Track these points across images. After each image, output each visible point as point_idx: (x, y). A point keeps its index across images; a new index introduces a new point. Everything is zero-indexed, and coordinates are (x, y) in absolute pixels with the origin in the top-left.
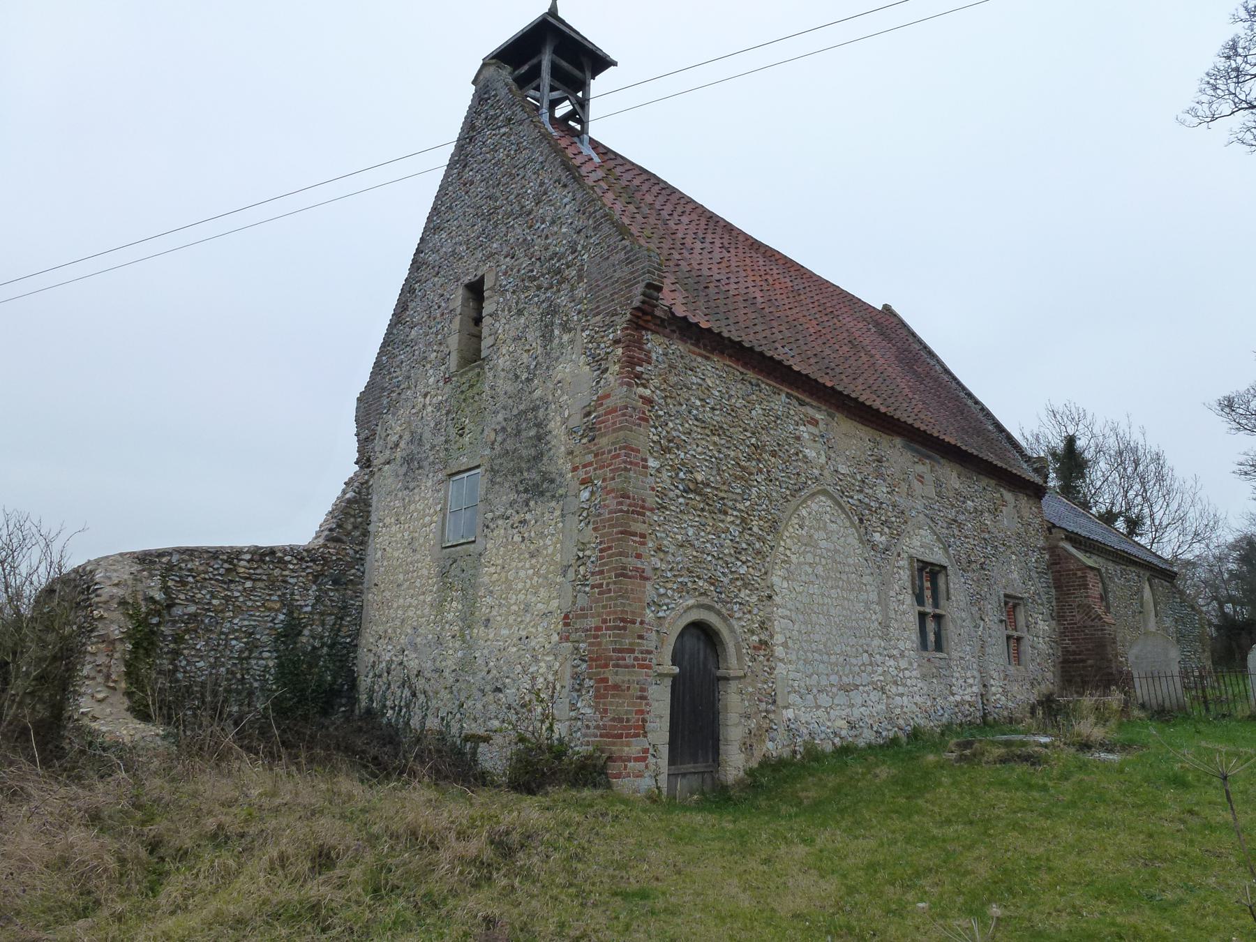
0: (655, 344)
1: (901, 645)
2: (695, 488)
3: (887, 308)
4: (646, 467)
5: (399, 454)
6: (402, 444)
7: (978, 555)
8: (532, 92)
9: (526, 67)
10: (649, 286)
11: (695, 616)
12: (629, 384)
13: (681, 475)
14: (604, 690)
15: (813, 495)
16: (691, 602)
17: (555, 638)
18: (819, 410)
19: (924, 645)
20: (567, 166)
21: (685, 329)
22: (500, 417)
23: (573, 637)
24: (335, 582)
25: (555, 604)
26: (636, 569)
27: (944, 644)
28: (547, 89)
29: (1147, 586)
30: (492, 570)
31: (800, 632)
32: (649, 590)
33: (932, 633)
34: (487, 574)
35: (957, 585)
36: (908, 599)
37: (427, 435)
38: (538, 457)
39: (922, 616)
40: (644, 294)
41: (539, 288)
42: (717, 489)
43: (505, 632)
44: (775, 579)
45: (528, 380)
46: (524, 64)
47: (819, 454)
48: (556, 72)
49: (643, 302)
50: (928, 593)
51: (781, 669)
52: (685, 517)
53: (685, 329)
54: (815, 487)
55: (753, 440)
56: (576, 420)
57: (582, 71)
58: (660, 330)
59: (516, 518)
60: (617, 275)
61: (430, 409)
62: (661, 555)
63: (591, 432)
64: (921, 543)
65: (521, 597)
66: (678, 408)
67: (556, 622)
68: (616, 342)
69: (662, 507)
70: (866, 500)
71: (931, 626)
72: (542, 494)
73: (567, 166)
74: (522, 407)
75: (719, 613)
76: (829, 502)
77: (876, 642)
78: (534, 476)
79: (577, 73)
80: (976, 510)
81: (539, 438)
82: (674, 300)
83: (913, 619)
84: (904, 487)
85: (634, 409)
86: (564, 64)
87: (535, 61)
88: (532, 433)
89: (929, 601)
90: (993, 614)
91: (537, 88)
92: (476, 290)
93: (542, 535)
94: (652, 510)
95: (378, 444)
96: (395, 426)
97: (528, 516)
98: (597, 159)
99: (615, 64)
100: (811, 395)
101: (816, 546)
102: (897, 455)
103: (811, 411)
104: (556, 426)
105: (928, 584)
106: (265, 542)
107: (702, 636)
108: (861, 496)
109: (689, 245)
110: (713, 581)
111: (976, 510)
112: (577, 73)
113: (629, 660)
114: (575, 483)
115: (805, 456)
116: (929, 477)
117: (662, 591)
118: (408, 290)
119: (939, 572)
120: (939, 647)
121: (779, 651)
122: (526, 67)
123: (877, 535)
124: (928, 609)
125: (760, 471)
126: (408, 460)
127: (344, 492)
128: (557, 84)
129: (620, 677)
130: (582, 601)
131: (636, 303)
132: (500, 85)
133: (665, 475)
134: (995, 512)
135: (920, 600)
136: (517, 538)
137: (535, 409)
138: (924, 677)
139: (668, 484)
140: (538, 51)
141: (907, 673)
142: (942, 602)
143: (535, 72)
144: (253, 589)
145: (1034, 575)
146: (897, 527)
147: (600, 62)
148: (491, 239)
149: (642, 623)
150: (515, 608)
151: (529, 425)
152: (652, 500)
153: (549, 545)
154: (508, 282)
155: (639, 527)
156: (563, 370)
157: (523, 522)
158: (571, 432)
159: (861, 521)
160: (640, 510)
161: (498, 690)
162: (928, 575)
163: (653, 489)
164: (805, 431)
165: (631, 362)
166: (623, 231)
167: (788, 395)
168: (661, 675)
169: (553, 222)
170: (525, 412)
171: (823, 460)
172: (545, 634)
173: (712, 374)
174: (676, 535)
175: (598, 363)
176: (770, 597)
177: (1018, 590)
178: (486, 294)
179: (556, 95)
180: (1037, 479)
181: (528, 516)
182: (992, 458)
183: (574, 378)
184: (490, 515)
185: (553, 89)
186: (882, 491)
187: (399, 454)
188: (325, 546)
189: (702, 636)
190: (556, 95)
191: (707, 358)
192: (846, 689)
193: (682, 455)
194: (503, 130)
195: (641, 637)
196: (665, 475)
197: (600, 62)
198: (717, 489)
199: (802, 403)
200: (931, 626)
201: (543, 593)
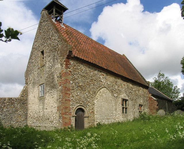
0: (72, 62)
1: (119, 112)
2: (80, 86)
3: (124, 55)
4: (70, 83)
5: (32, 82)
6: (32, 80)
7: (135, 98)
8: (52, 15)
9: (51, 10)
10: (69, 51)
11: (80, 107)
12: (67, 69)
13: (77, 84)
14: (64, 118)
15: (103, 88)
16: (79, 105)
17: (56, 111)
18: (104, 73)
19: (123, 112)
20: (57, 29)
21: (77, 59)
22: (47, 75)
23: (59, 110)
24: (23, 103)
25: (56, 106)
26: (68, 99)
27: (127, 112)
28: (54, 15)
29: (167, 103)
30: (47, 100)
31: (99, 110)
32: (71, 103)
33: (125, 109)
34: (46, 101)
35: (130, 103)
36: (121, 105)
37: (36, 78)
38: (53, 82)
39: (123, 108)
40: (69, 53)
41: (52, 52)
42: (84, 87)
43: (49, 110)
44: (95, 102)
45: (51, 68)
46: (50, 10)
47: (104, 81)
48: (56, 11)
49: (69, 54)
50: (124, 104)
51: (95, 116)
52: (78, 91)
53: (77, 59)
54: (103, 86)
55: (91, 78)
56: (59, 75)
57: (62, 11)
58: (72, 59)
59: (50, 92)
60: (65, 49)
61: (36, 74)
62: (73, 97)
63: (61, 77)
64: (123, 96)
65: (51, 105)
66: (76, 73)
67: (56, 109)
68: (65, 61)
69: (73, 89)
70: (113, 89)
71: (124, 109)
72: (54, 88)
73: (57, 29)
74: (50, 73)
75: (84, 107)
76: (106, 89)
77: (114, 112)
78: (52, 85)
79: (60, 11)
80: (135, 90)
81: (53, 78)
82: (75, 53)
83: (121, 108)
84: (121, 86)
85: (68, 73)
86: (58, 10)
87: (52, 9)
88: (52, 78)
89: (124, 105)
90: (137, 106)
91: (53, 15)
92: (42, 53)
93: (54, 94)
94: (71, 90)
95: (28, 80)
96: (31, 77)
97: (52, 91)
98: (65, 28)
99: (68, 9)
100: (103, 70)
101: (103, 96)
102: (120, 81)
103: (103, 73)
104: (56, 76)
105: (124, 103)
106: (11, 97)
107: (81, 110)
108: (112, 88)
109: (82, 43)
110: (83, 102)
111: (135, 90)
112: (60, 11)
113: (67, 114)
114: (59, 86)
115: (101, 81)
116: (126, 85)
117: (73, 103)
118: (32, 53)
119: (127, 101)
120: (126, 113)
121: (95, 113)
122: (51, 10)
123: (115, 95)
124: (124, 107)
125: (92, 83)
126: (33, 83)
127: (23, 89)
128: (57, 13)
129: (66, 116)
130: (60, 105)
131: (67, 54)
132: (45, 14)
133: (74, 84)
134: (139, 91)
135: (123, 105)
136: (50, 95)
137: (52, 73)
138: (123, 117)
139: (74, 85)
140: (53, 7)
141: (120, 117)
142: (127, 106)
143: (52, 12)
144: (9, 104)
145: (145, 101)
146: (119, 92)
147: (65, 9)
148: (45, 43)
149: (70, 108)
150: (50, 106)
151: (51, 75)
152: (71, 88)
153: (55, 96)
154: (48, 51)
155: (69, 93)
156: (56, 66)
157: (51, 92)
158: (58, 77)
159: (112, 92)
160: (69, 90)
161: (48, 119)
162: (124, 101)
163: (71, 86)
164: (101, 77)
165: (67, 65)
166: (66, 41)
167: (98, 70)
168: (73, 116)
169: (54, 40)
170: (51, 74)
171: (105, 82)
172: (55, 110)
173: (83, 68)
174: (76, 94)
175: (61, 65)
176: (94, 105)
177: (142, 104)
178: (44, 53)
179: (56, 16)
180: (148, 85)
181: (52, 91)
182: (138, 81)
183: (58, 67)
184: (46, 92)
185: (56, 14)
186: (116, 87)
187: (32, 82)
188: (20, 97)
189: (81, 110)
190: (56, 16)
191: (82, 64)
192: (108, 119)
193: (77, 81)
194: (46, 23)
195: (69, 110)
196: (74, 84)
197: (65, 9)
198: (84, 87)
199: (101, 72)
200: (124, 109)
201: (54, 104)
